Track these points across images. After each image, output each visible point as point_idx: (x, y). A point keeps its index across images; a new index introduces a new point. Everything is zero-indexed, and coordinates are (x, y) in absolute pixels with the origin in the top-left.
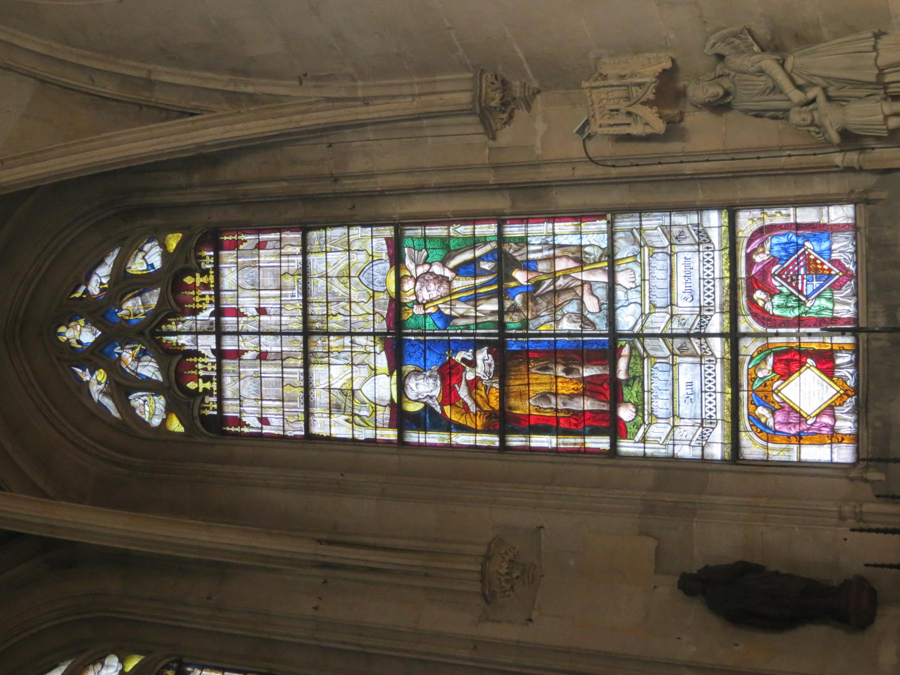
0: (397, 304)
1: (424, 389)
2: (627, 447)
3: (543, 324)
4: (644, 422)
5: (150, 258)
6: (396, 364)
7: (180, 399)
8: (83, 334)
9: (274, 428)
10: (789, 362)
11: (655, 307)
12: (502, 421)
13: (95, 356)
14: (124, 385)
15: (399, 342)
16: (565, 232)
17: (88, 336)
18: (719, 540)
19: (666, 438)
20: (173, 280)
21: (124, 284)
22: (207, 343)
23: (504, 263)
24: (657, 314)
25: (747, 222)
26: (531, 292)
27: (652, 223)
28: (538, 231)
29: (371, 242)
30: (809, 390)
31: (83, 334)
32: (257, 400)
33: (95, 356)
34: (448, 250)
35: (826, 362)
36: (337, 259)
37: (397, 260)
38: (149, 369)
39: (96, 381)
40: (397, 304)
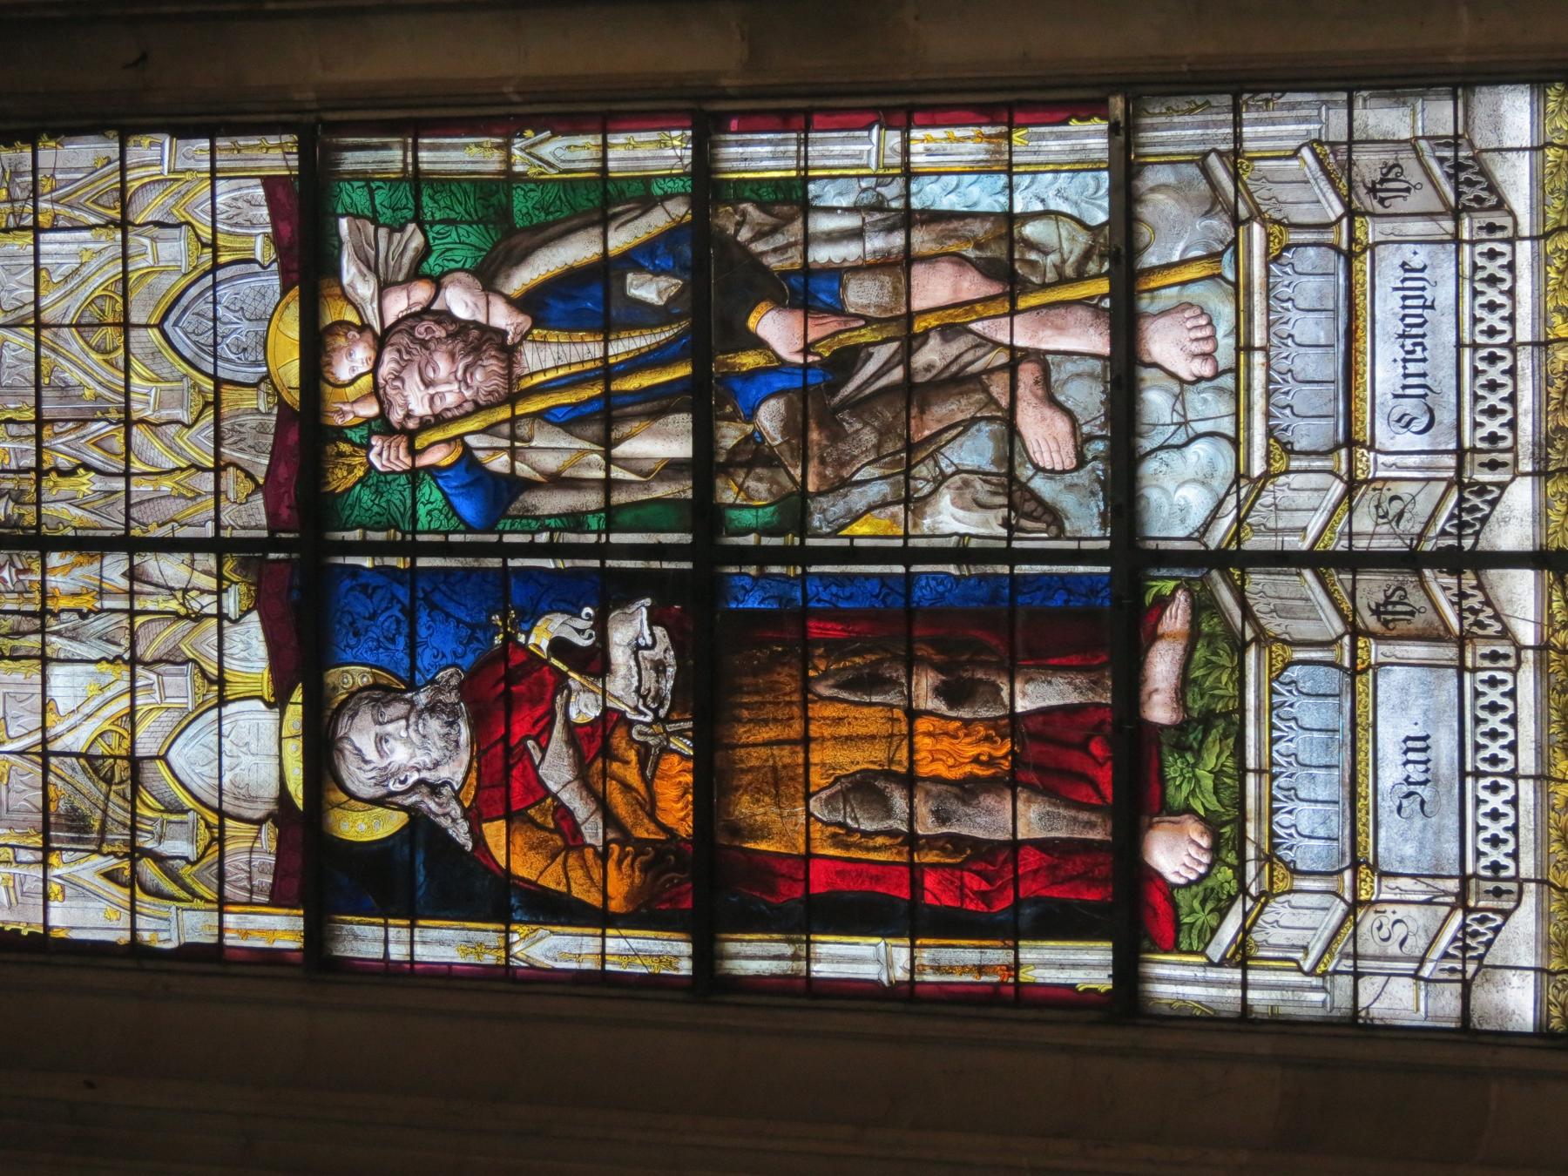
0: (306, 432)
1: (404, 753)
2: (1178, 981)
3: (863, 514)
4: (1243, 890)
6: (300, 665)
11: (1289, 450)
12: (706, 881)
15: (322, 576)
16: (950, 165)
19: (1327, 948)
24: (1296, 899)
26: (819, 389)
28: (849, 155)
34: (501, 224)
37: (307, 263)
40: (306, 432)
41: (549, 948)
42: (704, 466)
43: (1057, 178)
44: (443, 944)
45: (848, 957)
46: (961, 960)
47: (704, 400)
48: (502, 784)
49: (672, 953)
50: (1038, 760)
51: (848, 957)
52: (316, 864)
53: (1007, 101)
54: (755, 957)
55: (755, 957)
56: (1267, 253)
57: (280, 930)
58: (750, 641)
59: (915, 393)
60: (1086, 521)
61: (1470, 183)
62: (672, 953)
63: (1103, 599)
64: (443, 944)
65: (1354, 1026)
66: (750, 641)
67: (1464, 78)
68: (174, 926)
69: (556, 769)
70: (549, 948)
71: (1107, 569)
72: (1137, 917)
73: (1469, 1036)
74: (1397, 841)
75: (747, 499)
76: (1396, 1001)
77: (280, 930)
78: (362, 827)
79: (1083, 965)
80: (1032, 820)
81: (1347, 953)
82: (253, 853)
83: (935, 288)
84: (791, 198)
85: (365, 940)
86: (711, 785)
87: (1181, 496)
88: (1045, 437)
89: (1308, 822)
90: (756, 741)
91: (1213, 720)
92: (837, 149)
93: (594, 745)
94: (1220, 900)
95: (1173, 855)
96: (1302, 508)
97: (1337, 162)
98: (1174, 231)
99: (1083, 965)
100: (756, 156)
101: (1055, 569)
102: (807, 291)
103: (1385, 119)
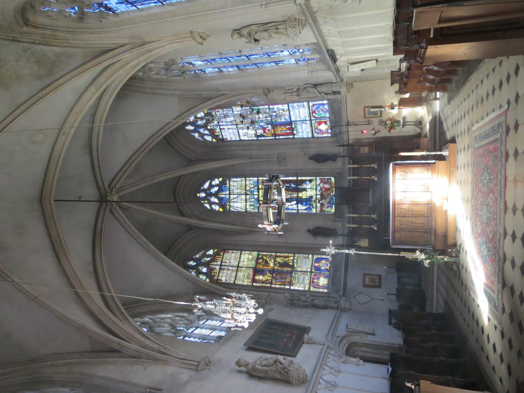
2: (292, 288)
3: (279, 121)
8: (203, 195)
9: (234, 139)
10: (320, 123)
12: (275, 135)
14: (202, 135)
16: (280, 106)
18: (314, 150)
20: (221, 186)
21: (211, 186)
25: (311, 104)
26: (276, 116)
27: (295, 105)
28: (275, 107)
30: (323, 127)
31: (203, 195)
33: (204, 199)
35: (326, 123)
38: (216, 200)
39: (196, 135)
41: (267, 138)
42: (271, 119)
43: (285, 107)
44: (263, 138)
45: (281, 137)
46: (287, 137)
47: (271, 116)
48: (265, 132)
49: (274, 138)
50: (288, 129)
51: (281, 137)
53: (283, 104)
54: (277, 137)
55: (277, 137)
56: (310, 383)
57: (256, 138)
58: (275, 126)
59: (280, 116)
60: (289, 120)
61: (304, 106)
62: (274, 138)
64: (263, 138)
65: (303, 138)
66: (275, 126)
67: (303, 102)
68: (250, 139)
69: (267, 131)
70: (267, 138)
71: (432, 36)
72: (294, 135)
73: (308, 138)
74: (304, 131)
75: (273, 120)
76: (305, 137)
77: (256, 138)
78: (258, 134)
79: (292, 137)
80: (288, 131)
81: (303, 135)
82: (254, 136)
83: (280, 112)
84: (273, 108)
85: (260, 138)
86: (274, 131)
87: (293, 119)
88: (287, 117)
89: (300, 130)
90: (276, 130)
91: (296, 127)
93: (269, 130)
95: (295, 132)
96: (298, 119)
97: (298, 106)
98: (291, 109)
99: (292, 137)
100: (271, 107)
101: (138, 187)
102: (275, 112)
103: (299, 104)
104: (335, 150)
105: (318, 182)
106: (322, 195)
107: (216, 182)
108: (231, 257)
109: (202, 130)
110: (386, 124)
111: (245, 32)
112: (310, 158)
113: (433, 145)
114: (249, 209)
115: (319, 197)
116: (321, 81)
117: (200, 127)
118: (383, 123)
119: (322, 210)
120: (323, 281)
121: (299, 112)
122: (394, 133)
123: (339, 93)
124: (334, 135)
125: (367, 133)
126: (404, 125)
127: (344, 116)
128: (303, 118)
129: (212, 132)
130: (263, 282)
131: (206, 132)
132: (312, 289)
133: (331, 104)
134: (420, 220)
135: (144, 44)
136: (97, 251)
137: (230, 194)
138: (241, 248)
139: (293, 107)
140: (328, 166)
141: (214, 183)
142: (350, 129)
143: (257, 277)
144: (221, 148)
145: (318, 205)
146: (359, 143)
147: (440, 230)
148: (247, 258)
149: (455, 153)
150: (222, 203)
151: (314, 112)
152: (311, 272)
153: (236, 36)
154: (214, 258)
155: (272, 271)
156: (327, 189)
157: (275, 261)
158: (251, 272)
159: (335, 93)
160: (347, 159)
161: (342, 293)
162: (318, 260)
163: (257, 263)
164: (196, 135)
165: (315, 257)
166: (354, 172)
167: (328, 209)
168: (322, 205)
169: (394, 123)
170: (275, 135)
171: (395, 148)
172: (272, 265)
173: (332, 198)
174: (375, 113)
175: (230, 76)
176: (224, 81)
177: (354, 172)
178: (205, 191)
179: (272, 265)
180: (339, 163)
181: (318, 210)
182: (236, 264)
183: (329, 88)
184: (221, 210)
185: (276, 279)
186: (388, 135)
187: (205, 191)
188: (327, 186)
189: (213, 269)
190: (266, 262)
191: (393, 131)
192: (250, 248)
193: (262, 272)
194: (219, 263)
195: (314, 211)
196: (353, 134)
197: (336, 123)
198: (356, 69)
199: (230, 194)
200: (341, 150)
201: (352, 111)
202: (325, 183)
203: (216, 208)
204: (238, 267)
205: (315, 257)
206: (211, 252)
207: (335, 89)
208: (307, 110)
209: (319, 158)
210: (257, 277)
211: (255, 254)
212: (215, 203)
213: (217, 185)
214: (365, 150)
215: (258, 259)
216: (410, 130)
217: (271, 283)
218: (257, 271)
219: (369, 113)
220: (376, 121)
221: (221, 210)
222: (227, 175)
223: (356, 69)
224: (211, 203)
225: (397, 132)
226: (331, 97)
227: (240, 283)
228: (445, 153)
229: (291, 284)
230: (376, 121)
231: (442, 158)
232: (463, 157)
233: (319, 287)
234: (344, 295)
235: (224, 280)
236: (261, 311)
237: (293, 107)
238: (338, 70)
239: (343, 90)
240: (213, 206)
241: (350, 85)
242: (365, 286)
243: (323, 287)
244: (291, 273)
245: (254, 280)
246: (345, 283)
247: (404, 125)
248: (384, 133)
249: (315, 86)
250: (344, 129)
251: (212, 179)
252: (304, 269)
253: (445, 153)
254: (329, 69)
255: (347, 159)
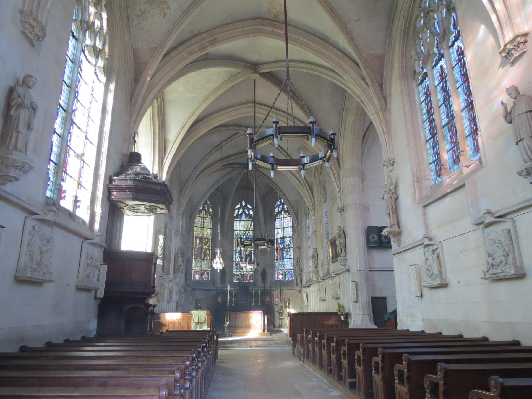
0: (286, 237)
1: (279, 241)
3: (285, 252)
5: (251, 213)
6: (281, 238)
7: (278, 213)
8: (244, 204)
9: (276, 225)
10: (282, 275)
12: (277, 249)
13: (241, 205)
14: (278, 206)
15: (283, 238)
16: (292, 254)
17: (282, 201)
18: (268, 271)
20: (248, 216)
21: (248, 209)
22: (282, 216)
23: (289, 248)
25: (292, 271)
26: (287, 251)
27: (292, 262)
28: (292, 251)
29: (291, 235)
30: (280, 276)
31: (244, 204)
32: (278, 223)
33: (241, 205)
34: (290, 242)
35: (283, 278)
36: (290, 230)
37: (290, 237)
38: (240, 212)
39: (278, 203)
40: (286, 237)
43: (292, 257)
52: (277, 239)
53: (293, 255)
58: (282, 249)
63: (283, 259)
66: (282, 249)
92: (401, 23)
94: (256, 133)
104: (268, 283)
105: (251, 273)
106: (244, 275)
107: (251, 213)
108: (208, 223)
109: (281, 207)
110: (280, 310)
111: (316, 254)
112: (264, 269)
113: (271, 326)
114: (235, 233)
115: (243, 273)
116: (303, 278)
117: (283, 206)
118: (281, 308)
119: (235, 275)
120: (197, 277)
121: (289, 264)
122: (276, 314)
123: (297, 286)
124: (276, 282)
125: (277, 300)
126: (280, 319)
127: (285, 288)
128: (286, 266)
129: (279, 213)
130: (196, 243)
131: (280, 210)
132: (193, 271)
133: (292, 281)
134: (240, 323)
135: (314, 209)
136: (215, 150)
137: (244, 221)
138: (214, 228)
139: (291, 261)
140: (259, 278)
141: (251, 211)
142: (279, 291)
143: (198, 239)
144: (271, 218)
145: (238, 273)
146: (271, 295)
147: (236, 331)
148: (208, 232)
149: (266, 335)
150: (239, 216)
151: (288, 272)
152: (202, 270)
153: (314, 250)
154: (208, 212)
155: (201, 248)
156: (246, 278)
157: (207, 249)
158: (201, 236)
159: (297, 284)
160: (263, 289)
161: (193, 288)
162: (208, 274)
163: (206, 239)
164: (278, 203)
165: (210, 272)
166: (256, 294)
167: (235, 279)
168: (238, 275)
169: (281, 314)
170: (277, 249)
171: (269, 311)
172: (205, 247)
173: (242, 280)
174: (286, 304)
175: (306, 232)
176: (304, 228)
177: (256, 294)
178: (246, 205)
179: (205, 247)
180: (260, 284)
181: (235, 273)
182: (205, 226)
183: (298, 282)
184: (235, 215)
185: (198, 250)
186: (275, 311)
187: (246, 205)
188: (248, 278)
189: (201, 212)
190: (206, 244)
191: (277, 313)
192: (214, 234)
193: (201, 242)
194: (205, 216)
195: (235, 271)
196: (276, 293)
197: (283, 284)
198: (305, 296)
199: (244, 221)
200: (268, 286)
201: (288, 292)
202: (250, 277)
203: (236, 213)
204: (203, 228)
205: (210, 272)
206: (211, 210)
207: (298, 284)
208: (290, 268)
209: (264, 274)
210: (198, 239)
211: (210, 237)
212: (239, 211)
213: (249, 213)
214: (268, 300)
215: (208, 239)
216: (277, 322)
217: (195, 248)
218: (201, 239)
219: (286, 301)
220: (283, 304)
221: (235, 215)
222: (255, 219)
223: (305, 296)
224: (239, 209)
225: (277, 315)
226: (295, 282)
227: (195, 230)
228: (266, 332)
229: (195, 259)
230: (283, 304)
231: (264, 331)
232: (267, 336)
233: (194, 275)
234: (193, 289)
235: (197, 220)
236: (218, 271)
237: (291, 261)
238: (305, 287)
239: (298, 288)
240: (237, 211)
241: (300, 292)
242: (197, 300)
243: (194, 277)
244: (201, 259)
245: (196, 238)
246: (197, 289)
247: (280, 319)
248: (276, 309)
249: (301, 274)
250: (279, 288)
251: (253, 210)
252: (203, 266)
253: (266, 332)
254: (307, 283)
255: (263, 289)
